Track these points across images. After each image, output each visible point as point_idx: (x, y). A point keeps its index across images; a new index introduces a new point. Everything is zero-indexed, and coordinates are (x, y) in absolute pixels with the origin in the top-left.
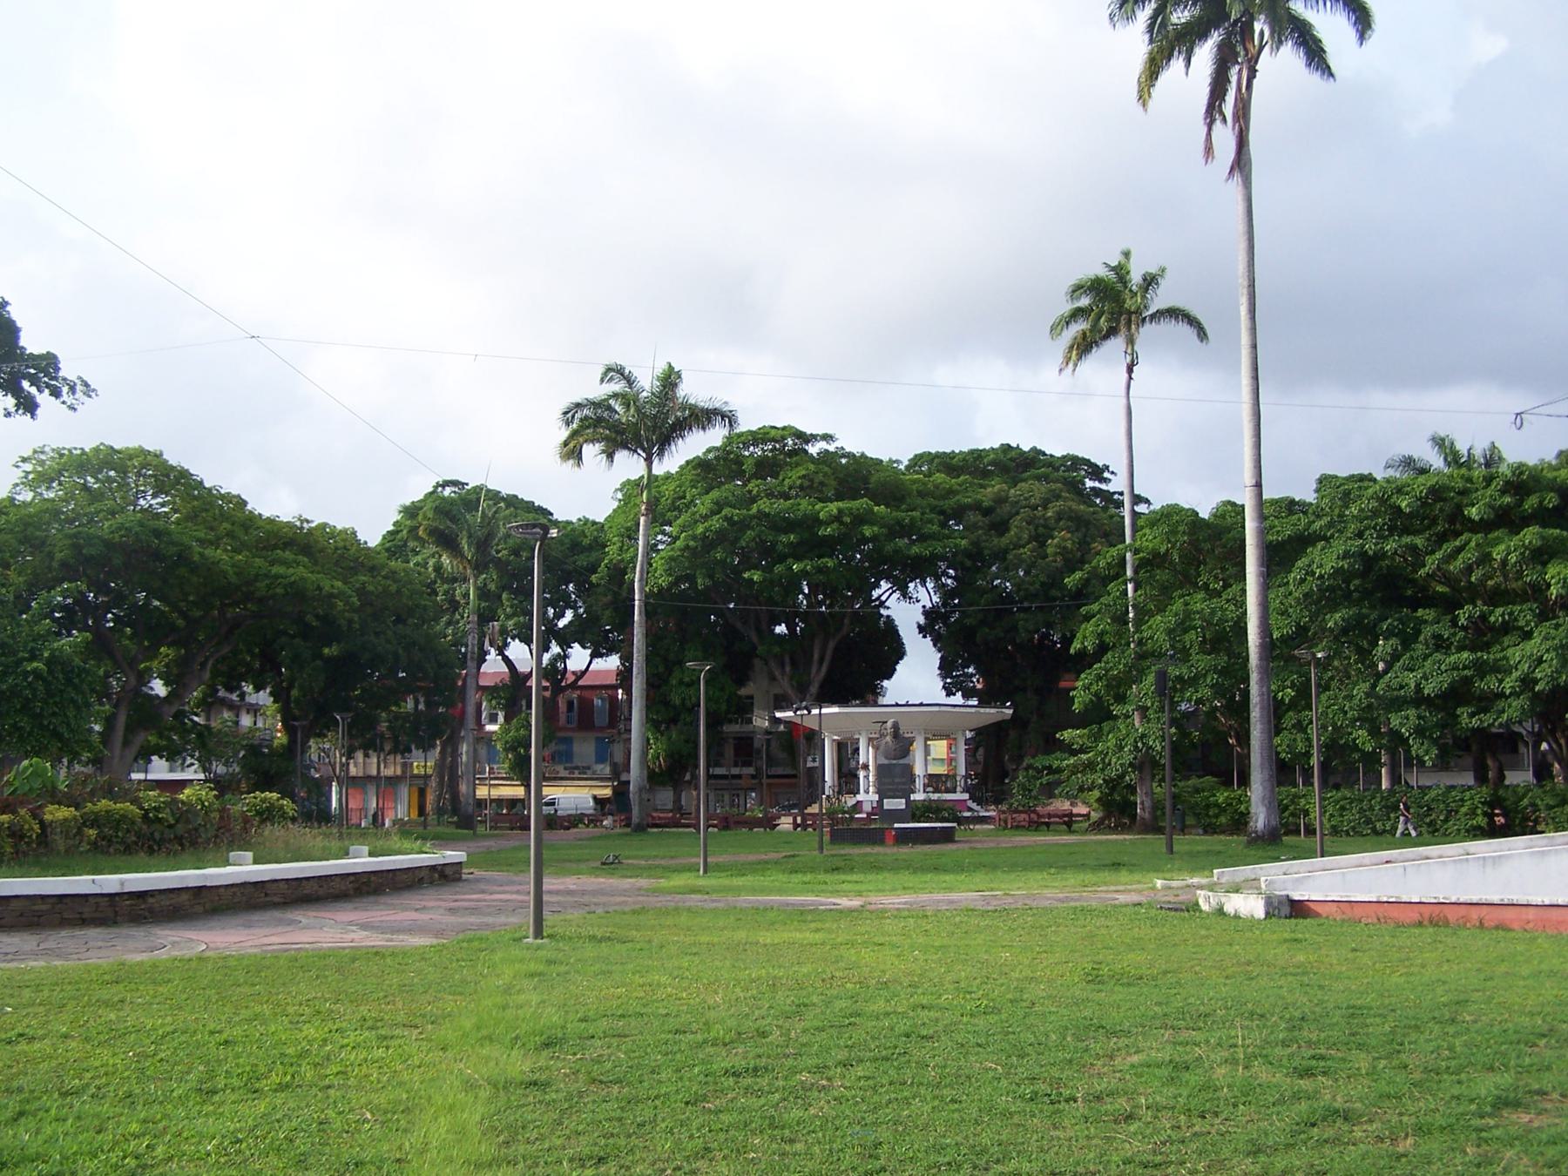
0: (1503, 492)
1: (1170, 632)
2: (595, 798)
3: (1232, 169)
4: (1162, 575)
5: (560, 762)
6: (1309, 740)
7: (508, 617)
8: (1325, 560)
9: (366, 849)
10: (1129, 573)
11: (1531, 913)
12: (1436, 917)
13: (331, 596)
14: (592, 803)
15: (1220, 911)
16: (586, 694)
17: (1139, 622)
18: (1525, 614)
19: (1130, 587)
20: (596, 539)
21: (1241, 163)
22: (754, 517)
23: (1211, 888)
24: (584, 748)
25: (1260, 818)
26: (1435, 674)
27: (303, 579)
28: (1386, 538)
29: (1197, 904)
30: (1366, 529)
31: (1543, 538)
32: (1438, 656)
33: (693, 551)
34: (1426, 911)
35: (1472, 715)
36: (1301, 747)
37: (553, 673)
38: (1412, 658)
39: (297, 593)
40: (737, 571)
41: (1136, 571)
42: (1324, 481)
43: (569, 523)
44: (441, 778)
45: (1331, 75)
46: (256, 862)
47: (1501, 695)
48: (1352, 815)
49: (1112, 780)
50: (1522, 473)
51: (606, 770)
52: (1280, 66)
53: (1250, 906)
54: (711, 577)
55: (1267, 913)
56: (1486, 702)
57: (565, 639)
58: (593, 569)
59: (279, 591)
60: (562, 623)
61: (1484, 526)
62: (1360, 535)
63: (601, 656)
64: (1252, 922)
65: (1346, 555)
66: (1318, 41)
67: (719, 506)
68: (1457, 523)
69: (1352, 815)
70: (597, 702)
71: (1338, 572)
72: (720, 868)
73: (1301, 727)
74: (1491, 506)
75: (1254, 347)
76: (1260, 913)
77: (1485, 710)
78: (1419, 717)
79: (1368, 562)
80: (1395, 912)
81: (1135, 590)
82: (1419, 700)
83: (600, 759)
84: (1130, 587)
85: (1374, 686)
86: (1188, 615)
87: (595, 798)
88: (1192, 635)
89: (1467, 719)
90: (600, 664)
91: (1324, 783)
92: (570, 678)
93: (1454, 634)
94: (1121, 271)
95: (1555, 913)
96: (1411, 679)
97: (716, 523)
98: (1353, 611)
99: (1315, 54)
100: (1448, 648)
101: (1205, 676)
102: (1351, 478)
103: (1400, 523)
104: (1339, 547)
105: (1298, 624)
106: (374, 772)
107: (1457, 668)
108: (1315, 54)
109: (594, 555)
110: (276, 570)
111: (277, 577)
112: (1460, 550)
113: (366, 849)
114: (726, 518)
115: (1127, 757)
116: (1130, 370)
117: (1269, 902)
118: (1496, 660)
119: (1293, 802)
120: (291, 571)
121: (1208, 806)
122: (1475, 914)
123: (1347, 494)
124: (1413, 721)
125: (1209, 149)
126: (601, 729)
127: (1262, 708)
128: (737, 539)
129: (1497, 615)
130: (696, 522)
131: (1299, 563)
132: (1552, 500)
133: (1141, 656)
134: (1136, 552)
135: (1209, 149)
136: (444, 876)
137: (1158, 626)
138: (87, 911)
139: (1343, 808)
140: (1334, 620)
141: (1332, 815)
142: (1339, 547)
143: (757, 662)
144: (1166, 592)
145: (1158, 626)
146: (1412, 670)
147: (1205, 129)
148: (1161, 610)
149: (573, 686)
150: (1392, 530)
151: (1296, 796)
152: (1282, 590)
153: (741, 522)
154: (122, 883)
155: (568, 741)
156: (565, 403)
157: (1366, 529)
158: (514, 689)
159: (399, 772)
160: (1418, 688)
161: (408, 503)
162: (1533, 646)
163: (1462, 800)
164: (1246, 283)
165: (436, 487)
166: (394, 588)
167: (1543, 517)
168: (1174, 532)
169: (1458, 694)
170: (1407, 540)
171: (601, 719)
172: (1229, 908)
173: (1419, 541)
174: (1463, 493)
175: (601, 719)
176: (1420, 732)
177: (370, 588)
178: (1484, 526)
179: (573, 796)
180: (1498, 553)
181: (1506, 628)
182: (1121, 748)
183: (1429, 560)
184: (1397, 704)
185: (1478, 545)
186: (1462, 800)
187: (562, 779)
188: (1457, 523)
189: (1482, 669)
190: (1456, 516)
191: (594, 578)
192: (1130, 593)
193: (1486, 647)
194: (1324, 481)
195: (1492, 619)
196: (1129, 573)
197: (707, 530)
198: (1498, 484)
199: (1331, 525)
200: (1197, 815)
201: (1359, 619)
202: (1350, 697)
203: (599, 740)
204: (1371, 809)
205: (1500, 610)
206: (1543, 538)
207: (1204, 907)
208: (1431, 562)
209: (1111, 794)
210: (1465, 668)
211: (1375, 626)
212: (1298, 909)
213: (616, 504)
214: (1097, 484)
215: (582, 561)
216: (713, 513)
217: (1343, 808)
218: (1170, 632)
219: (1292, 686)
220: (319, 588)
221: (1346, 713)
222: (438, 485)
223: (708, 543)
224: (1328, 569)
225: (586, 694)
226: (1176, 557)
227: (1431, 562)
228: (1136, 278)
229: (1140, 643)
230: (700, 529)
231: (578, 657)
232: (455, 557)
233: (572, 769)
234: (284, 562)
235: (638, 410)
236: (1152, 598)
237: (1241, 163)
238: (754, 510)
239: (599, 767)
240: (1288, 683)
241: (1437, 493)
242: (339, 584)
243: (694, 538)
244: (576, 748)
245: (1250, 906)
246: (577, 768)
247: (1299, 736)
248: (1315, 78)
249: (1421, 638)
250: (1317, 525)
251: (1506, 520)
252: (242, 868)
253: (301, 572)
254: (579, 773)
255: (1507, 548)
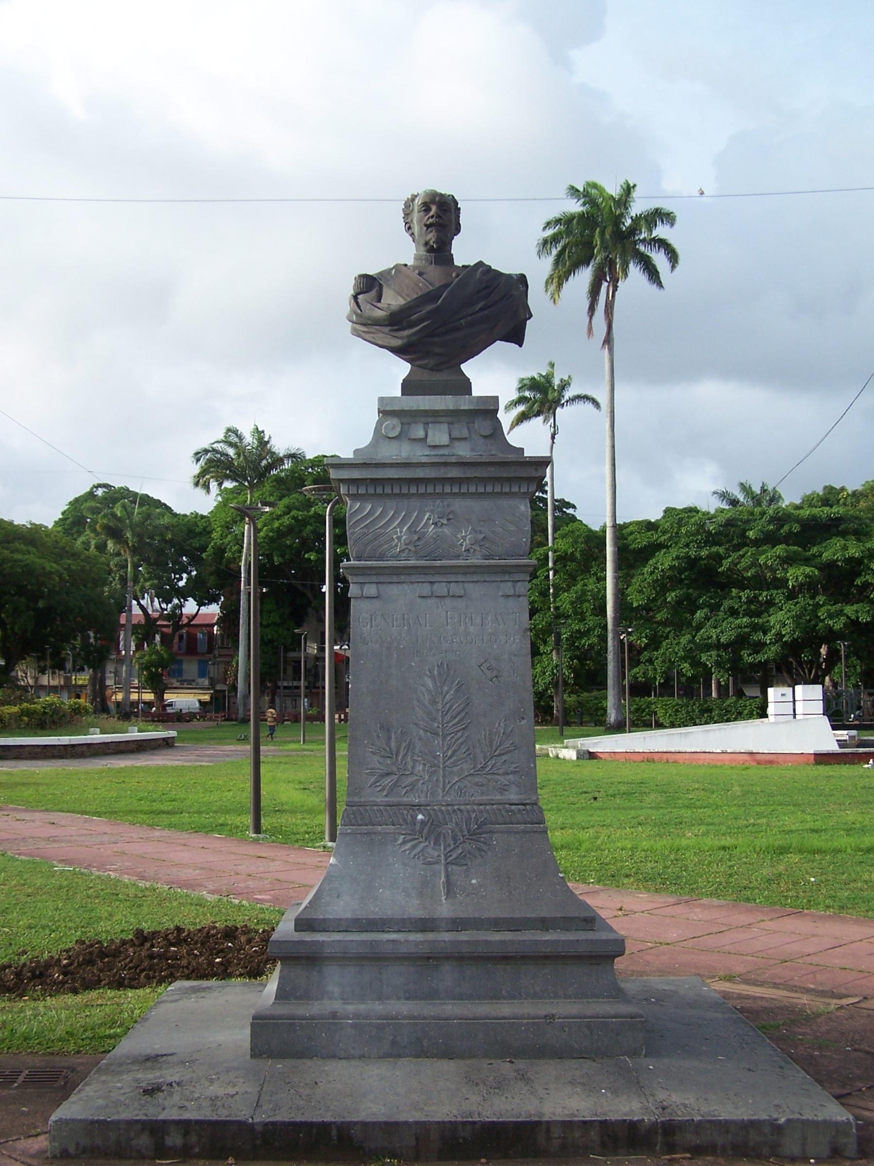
0: (769, 522)
1: (572, 603)
2: (200, 701)
3: (604, 341)
4: (571, 566)
5: (174, 677)
6: (655, 669)
7: (146, 580)
8: (665, 561)
9: (136, 729)
10: (551, 565)
11: (687, 756)
12: (649, 758)
13: (51, 573)
14: (198, 705)
15: (557, 757)
16: (192, 630)
17: (556, 595)
18: (779, 596)
19: (551, 573)
20: (205, 529)
21: (608, 340)
22: (311, 517)
23: (555, 747)
24: (190, 667)
25: (612, 716)
26: (726, 630)
27: (33, 562)
28: (702, 548)
29: (548, 754)
30: (691, 542)
31: (787, 551)
32: (730, 619)
33: (272, 540)
34: (646, 755)
35: (749, 655)
36: (650, 674)
37: (175, 617)
38: (716, 620)
39: (29, 571)
40: (299, 553)
41: (555, 563)
42: (668, 511)
43: (185, 515)
44: (94, 686)
45: (660, 285)
46: (101, 733)
47: (765, 644)
48: (682, 714)
49: (540, 692)
50: (778, 512)
51: (206, 682)
52: (635, 277)
53: (570, 754)
54: (283, 556)
55: (578, 758)
56: (759, 647)
57: (183, 594)
58: (203, 549)
59: (19, 570)
60: (182, 584)
61: (757, 543)
62: (687, 545)
63: (204, 605)
64: (571, 761)
65: (678, 558)
66: (654, 267)
67: (289, 509)
68: (744, 542)
69: (682, 714)
70: (200, 636)
71: (672, 568)
72: (312, 742)
73: (650, 661)
74: (762, 532)
75: (613, 447)
76: (574, 758)
77: (757, 652)
78: (718, 656)
79: (692, 563)
80: (632, 757)
81: (554, 575)
82: (719, 646)
83: (202, 673)
84: (551, 573)
85: (694, 637)
86: (584, 592)
87: (200, 701)
88: (586, 605)
89: (747, 657)
90: (204, 610)
91: (631, 694)
92: (185, 621)
93: (741, 607)
94: (548, 378)
95: (696, 756)
96: (713, 633)
97: (286, 520)
98: (684, 591)
99: (653, 274)
100: (738, 614)
101: (594, 630)
102: (685, 510)
103: (712, 539)
104: (674, 552)
105: (649, 598)
106: (46, 683)
107: (741, 628)
108: (653, 274)
109: (203, 540)
110: (17, 556)
111: (16, 561)
112: (743, 556)
113: (136, 729)
114: (294, 518)
115: (548, 679)
116: (553, 437)
117: (578, 753)
118: (763, 622)
119: (648, 707)
120: (26, 557)
121: (597, 709)
122: (665, 756)
123: (681, 519)
124: (715, 658)
125: (590, 330)
126: (203, 654)
127: (614, 654)
128: (300, 531)
129: (764, 596)
130: (273, 519)
131: (651, 562)
132: (796, 528)
133: (558, 617)
134: (555, 551)
135: (590, 330)
136: (167, 744)
137: (566, 599)
138: (56, 752)
139: (677, 711)
140: (671, 597)
141: (670, 715)
142: (674, 552)
143: (310, 610)
144: (572, 579)
145: (566, 599)
146: (715, 627)
147: (588, 319)
148: (567, 590)
149: (188, 625)
150: (706, 542)
151: (650, 703)
152: (641, 577)
153: (303, 520)
154: (70, 740)
155: (180, 662)
156: (195, 452)
157: (691, 542)
158: (147, 629)
159: (62, 683)
160: (719, 640)
161: (72, 499)
162: (780, 615)
163: (745, 706)
164: (609, 410)
165: (92, 489)
166: (88, 567)
167: (786, 540)
168: (576, 542)
169: (742, 641)
170: (714, 549)
171: (202, 647)
172: (561, 756)
173: (721, 550)
174: (748, 521)
175: (202, 647)
176: (718, 664)
177: (74, 568)
178: (757, 543)
179: (183, 700)
180: (762, 560)
181: (770, 603)
182: (544, 673)
183: (724, 562)
184: (708, 647)
185: (752, 554)
186: (745, 706)
187: (175, 688)
188: (744, 542)
189: (755, 628)
190: (743, 535)
191: (204, 556)
192: (551, 577)
193: (759, 615)
194: (668, 511)
195: (760, 598)
196: (551, 565)
197: (281, 525)
198: (766, 518)
199: (670, 538)
200: (590, 715)
201: (688, 597)
202: (678, 644)
203: (200, 662)
204: (693, 711)
205: (765, 593)
206: (787, 551)
207: (551, 755)
208: (726, 563)
209: (539, 701)
210: (745, 627)
211: (696, 600)
212: (592, 756)
213: (215, 504)
214: (541, 495)
215: (196, 543)
216: (285, 514)
217: (677, 711)
218: (572, 603)
219: (646, 637)
220: (44, 568)
221: (677, 653)
222: (94, 487)
223: (281, 533)
224: (666, 566)
225: (192, 630)
226: (578, 555)
227: (726, 563)
228: (556, 382)
229: (557, 608)
230: (276, 524)
231: (190, 607)
232: (119, 543)
233: (182, 682)
234: (17, 551)
235: (245, 457)
236: (565, 580)
237: (608, 340)
238: (312, 512)
239: (200, 680)
240: (644, 635)
241: (730, 523)
242: (54, 565)
243: (272, 530)
244: (185, 666)
245: (570, 754)
246: (185, 681)
247: (650, 668)
248: (654, 287)
249: (722, 608)
250: (662, 539)
251: (769, 539)
252: (96, 737)
253: (32, 558)
254: (188, 684)
255: (769, 556)
